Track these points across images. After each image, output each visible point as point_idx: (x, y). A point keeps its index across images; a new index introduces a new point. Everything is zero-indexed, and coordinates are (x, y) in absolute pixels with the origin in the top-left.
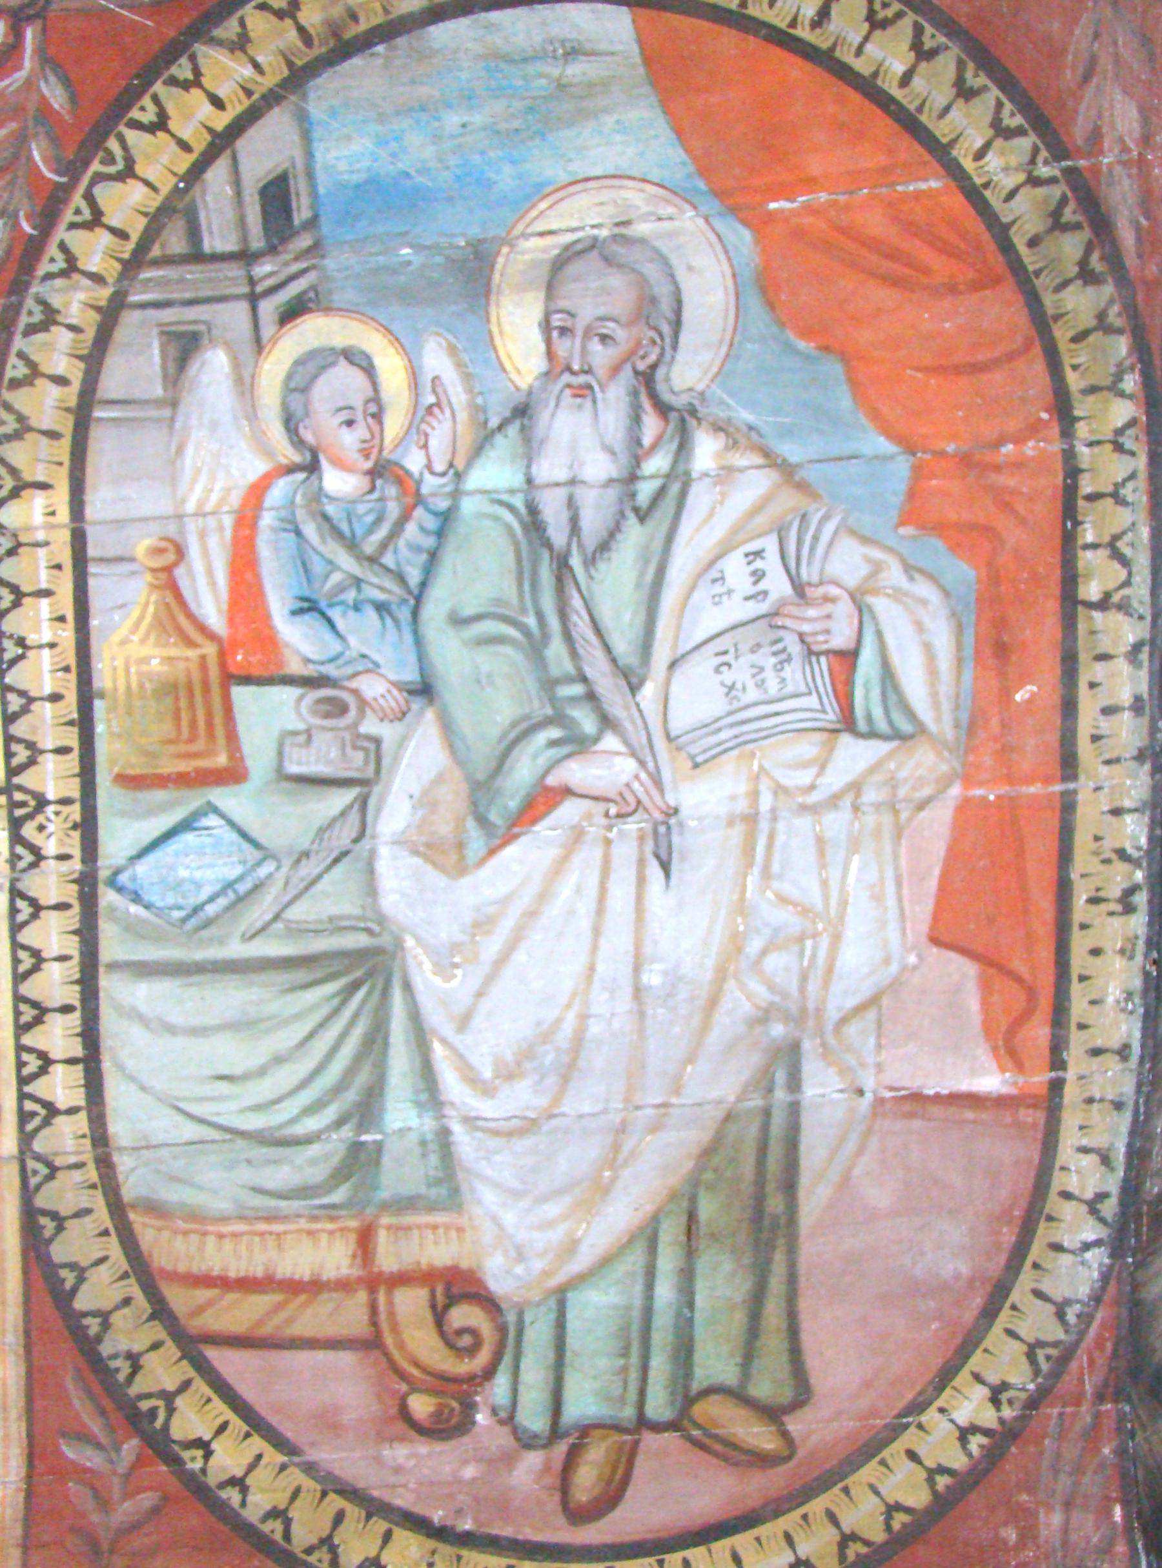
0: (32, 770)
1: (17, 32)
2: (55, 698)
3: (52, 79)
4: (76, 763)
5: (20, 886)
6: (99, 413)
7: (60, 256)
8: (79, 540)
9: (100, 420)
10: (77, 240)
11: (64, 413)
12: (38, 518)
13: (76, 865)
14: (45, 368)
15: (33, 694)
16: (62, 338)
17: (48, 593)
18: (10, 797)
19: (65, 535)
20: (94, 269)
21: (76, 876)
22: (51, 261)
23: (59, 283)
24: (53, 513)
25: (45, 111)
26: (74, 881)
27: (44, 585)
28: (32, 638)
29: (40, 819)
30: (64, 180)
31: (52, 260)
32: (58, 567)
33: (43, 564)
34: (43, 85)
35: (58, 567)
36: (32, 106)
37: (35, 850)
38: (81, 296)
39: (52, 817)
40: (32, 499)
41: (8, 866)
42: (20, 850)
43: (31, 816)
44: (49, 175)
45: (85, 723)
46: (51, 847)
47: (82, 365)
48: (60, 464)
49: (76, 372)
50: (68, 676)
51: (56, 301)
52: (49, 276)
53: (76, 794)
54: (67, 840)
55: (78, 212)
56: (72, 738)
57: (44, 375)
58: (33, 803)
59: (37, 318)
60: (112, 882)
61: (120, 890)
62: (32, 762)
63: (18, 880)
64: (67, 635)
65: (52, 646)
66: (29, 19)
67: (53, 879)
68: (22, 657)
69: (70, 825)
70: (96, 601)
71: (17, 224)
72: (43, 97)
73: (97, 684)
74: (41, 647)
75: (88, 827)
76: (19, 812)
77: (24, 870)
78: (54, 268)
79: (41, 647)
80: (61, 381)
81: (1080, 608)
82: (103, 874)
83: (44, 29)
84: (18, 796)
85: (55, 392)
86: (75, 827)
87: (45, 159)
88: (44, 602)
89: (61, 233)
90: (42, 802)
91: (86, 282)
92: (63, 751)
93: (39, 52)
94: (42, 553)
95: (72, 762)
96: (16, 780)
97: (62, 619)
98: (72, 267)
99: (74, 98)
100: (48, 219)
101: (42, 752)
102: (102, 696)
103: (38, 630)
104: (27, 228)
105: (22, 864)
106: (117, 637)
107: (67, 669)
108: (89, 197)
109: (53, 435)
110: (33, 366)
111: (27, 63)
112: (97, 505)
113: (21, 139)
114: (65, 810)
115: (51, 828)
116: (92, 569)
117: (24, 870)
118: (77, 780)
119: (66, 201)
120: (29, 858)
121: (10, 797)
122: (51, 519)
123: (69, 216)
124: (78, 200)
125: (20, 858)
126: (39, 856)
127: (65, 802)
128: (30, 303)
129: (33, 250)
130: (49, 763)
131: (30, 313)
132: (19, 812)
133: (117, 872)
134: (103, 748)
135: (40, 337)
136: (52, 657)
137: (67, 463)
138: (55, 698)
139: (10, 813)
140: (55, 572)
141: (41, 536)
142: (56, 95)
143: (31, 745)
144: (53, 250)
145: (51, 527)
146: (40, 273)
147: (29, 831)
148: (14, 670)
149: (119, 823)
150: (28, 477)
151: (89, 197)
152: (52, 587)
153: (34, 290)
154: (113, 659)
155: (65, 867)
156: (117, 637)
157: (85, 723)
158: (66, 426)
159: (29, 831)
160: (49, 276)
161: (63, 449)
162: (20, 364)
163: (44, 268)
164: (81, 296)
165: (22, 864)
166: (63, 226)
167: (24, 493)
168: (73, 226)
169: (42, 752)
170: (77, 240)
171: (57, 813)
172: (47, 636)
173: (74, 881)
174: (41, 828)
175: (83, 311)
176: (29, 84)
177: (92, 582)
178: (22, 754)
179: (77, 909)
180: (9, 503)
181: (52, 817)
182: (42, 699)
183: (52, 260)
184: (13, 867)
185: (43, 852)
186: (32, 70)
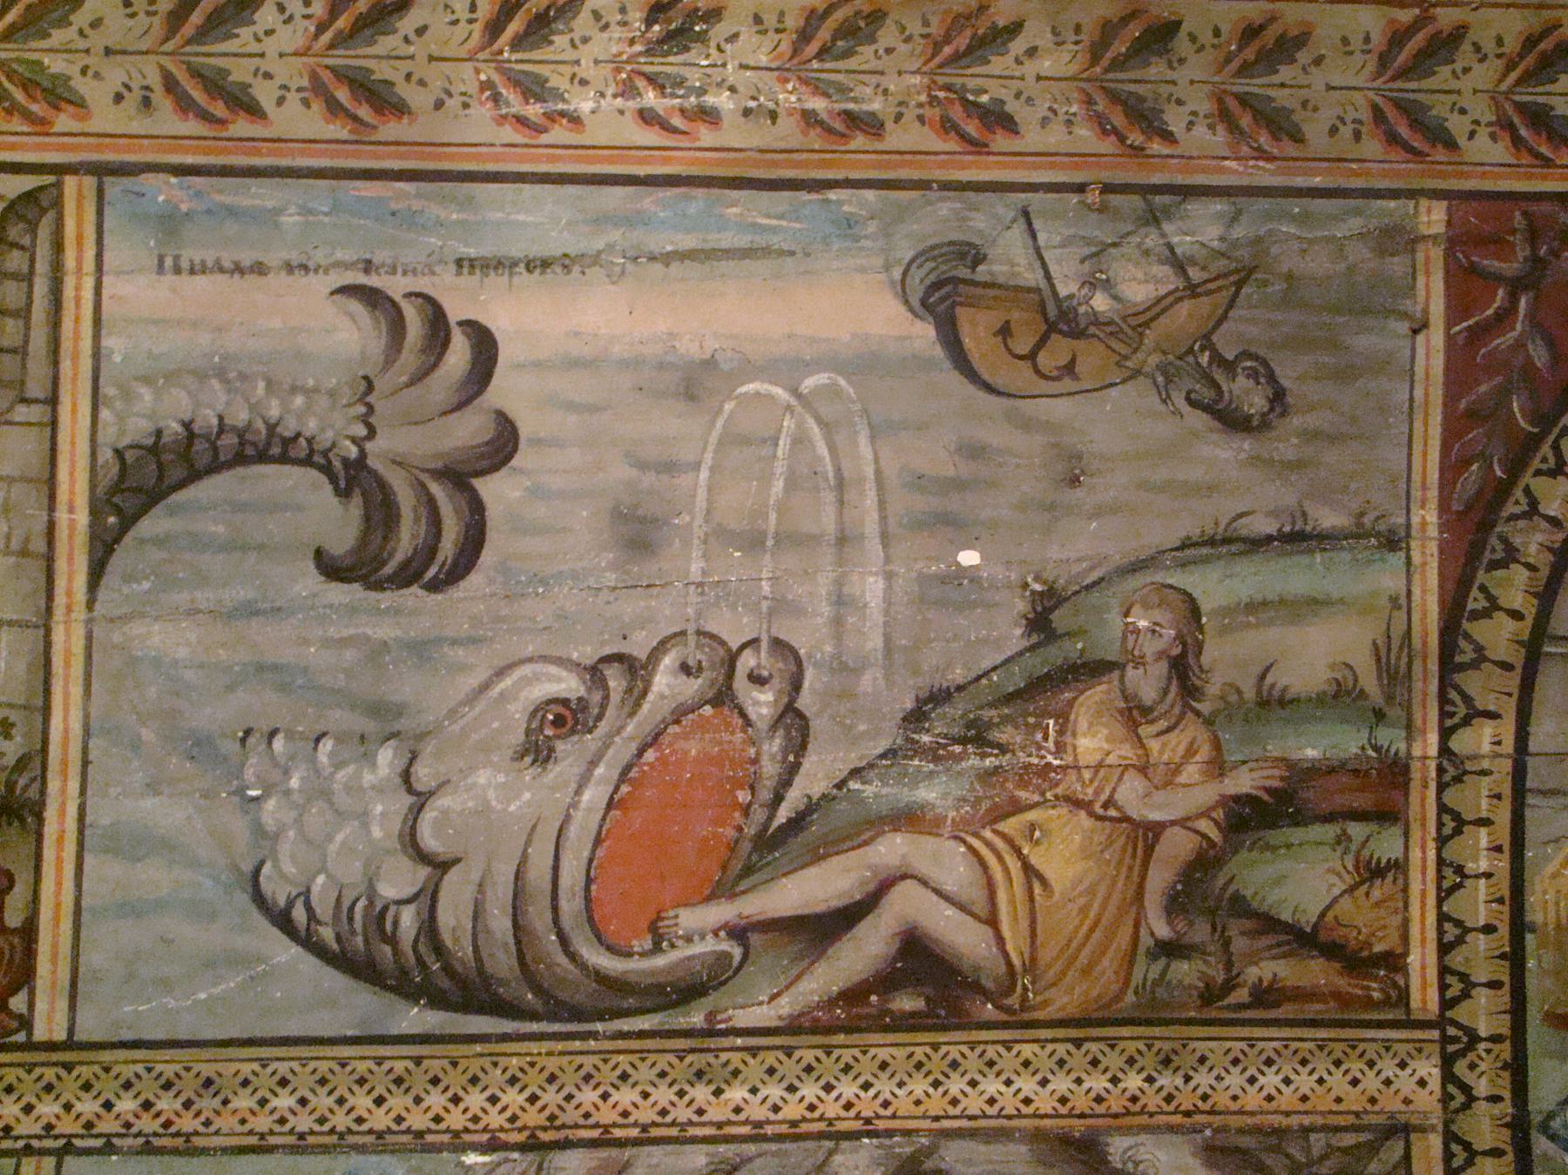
0: (1465, 1004)
1: (1513, 298)
2: (1489, 929)
3: (1539, 342)
4: (1507, 998)
5: (1454, 1128)
6: (1547, 649)
7: (1524, 500)
8: (1519, 773)
9: (1551, 654)
10: (1540, 485)
11: (1517, 647)
12: (1486, 748)
13: (1507, 1107)
14: (1502, 602)
15: (1469, 924)
16: (1519, 575)
17: (1484, 822)
18: (1443, 1031)
19: (1507, 765)
20: (1552, 514)
21: (1508, 1119)
22: (1516, 504)
23: (1521, 524)
24: (1499, 743)
25: (1528, 368)
26: (1506, 1125)
27: (1484, 814)
28: (1470, 867)
29: (1471, 1056)
30: (1536, 430)
31: (1517, 502)
32: (1498, 797)
33: (1485, 793)
34: (1530, 347)
35: (1498, 797)
36: (1519, 361)
37: (1466, 1089)
38: (1539, 537)
39: (1484, 1055)
40: (1481, 727)
41: (1440, 1106)
42: (1451, 1089)
43: (1462, 1053)
44: (1522, 423)
45: (1516, 958)
46: (1482, 1088)
47: (1535, 602)
48: (1510, 695)
49: (1530, 608)
50: (1500, 907)
51: (1517, 541)
52: (1514, 517)
53: (1506, 1031)
54: (1500, 1081)
55: (1545, 460)
56: (1503, 973)
57: (1501, 609)
58: (1465, 1039)
59: (1499, 555)
60: (1544, 1128)
61: (1553, 1138)
62: (1465, 995)
63: (1453, 1121)
64: (1503, 864)
65: (1488, 875)
66: (1526, 288)
67: (1486, 1125)
68: (1459, 886)
69: (1499, 1064)
70: (1532, 833)
71: (1491, 467)
72: (1529, 357)
73: (1529, 918)
74: (1477, 876)
75: (1518, 1069)
76: (1451, 1048)
77: (1457, 1111)
78: (1517, 510)
79: (1477, 876)
80: (1516, 615)
81: (14, 1160)
82: (1536, 1119)
83: (1536, 298)
84: (1452, 1031)
85: (1510, 625)
86: (1505, 1067)
87: (1522, 410)
88: (1483, 831)
89: (1527, 478)
90: (1474, 1038)
91: (1544, 525)
92: (1494, 985)
93: (1531, 316)
94: (1485, 780)
95: (1504, 997)
96: (1449, 1014)
97: (1498, 849)
98: (1533, 508)
99: (1556, 359)
100: (1516, 467)
101: (1475, 985)
102: (1533, 931)
103: (1476, 860)
104: (1499, 473)
105: (1455, 1104)
106: (1550, 869)
107: (1500, 901)
108: (1556, 448)
109: (1507, 667)
110: (1491, 598)
111: (1519, 326)
112: (1544, 734)
113: (1504, 393)
114: (1496, 1047)
115: (1483, 1066)
116: (1531, 800)
117: (1457, 1111)
118: (1508, 1017)
119: (1537, 449)
120: (1460, 1098)
121: (1443, 1031)
122: (1496, 748)
123: (1536, 463)
124: (1546, 449)
125: (1452, 1098)
126: (1471, 1099)
127: (1495, 1039)
128: (1494, 541)
129: (1503, 491)
130: (1482, 996)
131: (1493, 550)
132: (1451, 1048)
133: (1551, 1116)
134: (1532, 984)
135: (1499, 573)
136: (1487, 887)
137: (1516, 696)
138: (1489, 929)
139: (1443, 1049)
140: (1495, 801)
141: (1485, 764)
142: (1539, 355)
143: (1463, 977)
144: (1518, 493)
145: (1498, 755)
146: (1504, 514)
147: (1460, 1068)
148: (1452, 899)
149: (1549, 1064)
150: (1480, 706)
151: (1556, 448)
152: (1491, 816)
153: (1498, 529)
154: (1545, 892)
155: (1497, 1109)
156: (1550, 869)
157: (1516, 958)
158: (1517, 657)
159: (1460, 1068)
160: (1514, 517)
161: (1513, 681)
162: (1480, 596)
163: (1510, 509)
164: (1539, 537)
165: (1455, 1104)
166: (1530, 471)
167: (1474, 721)
168: (1538, 473)
169: (1475, 985)
170: (1540, 485)
171: (1488, 1051)
172: (1483, 865)
173: (1506, 1125)
174: (1472, 1066)
175: (1539, 552)
176: (1519, 345)
177: (1528, 813)
178: (1456, 988)
179: (1510, 1157)
180: (1461, 731)
181: (1484, 1055)
182: (1475, 929)
183: (1517, 502)
184: (1445, 1109)
185: (1474, 1093)
186: (1524, 330)
